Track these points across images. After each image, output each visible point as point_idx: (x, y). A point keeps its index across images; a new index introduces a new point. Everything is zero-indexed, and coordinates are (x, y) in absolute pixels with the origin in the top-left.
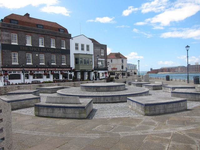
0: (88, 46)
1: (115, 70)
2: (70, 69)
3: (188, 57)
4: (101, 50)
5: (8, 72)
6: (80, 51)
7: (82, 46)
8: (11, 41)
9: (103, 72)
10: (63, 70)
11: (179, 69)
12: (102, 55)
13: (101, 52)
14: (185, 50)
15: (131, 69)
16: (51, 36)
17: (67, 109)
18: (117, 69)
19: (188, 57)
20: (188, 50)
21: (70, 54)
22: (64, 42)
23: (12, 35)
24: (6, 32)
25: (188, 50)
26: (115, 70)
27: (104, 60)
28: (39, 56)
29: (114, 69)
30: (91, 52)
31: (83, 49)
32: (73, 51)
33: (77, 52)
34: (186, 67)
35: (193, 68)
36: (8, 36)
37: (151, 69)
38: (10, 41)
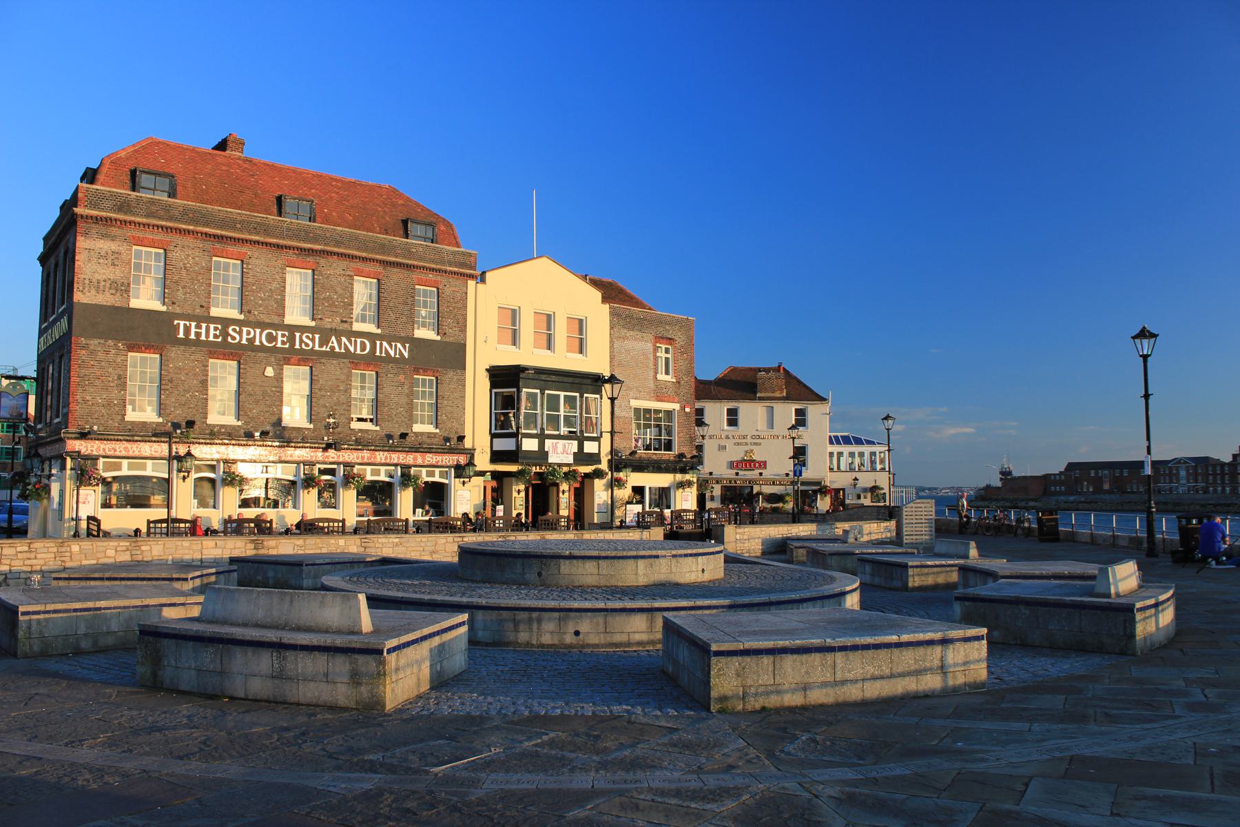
0: (580, 325)
1: (753, 474)
2: (463, 460)
3: (1147, 396)
4: (656, 349)
5: (102, 460)
6: (529, 355)
8: (127, 291)
9: (129, 408)
10: (419, 461)
11: (1183, 473)
12: (662, 377)
13: (656, 358)
14: (1130, 353)
15: (852, 470)
16: (360, 265)
17: (290, 655)
18: (763, 465)
19: (1147, 396)
20: (1145, 357)
22: (426, 294)
23: (138, 255)
24: (104, 236)
25: (1145, 357)
26: (753, 474)
27: (677, 406)
28: (279, 378)
29: (749, 464)
33: (508, 357)
34: (1223, 465)
35: (1223, 474)
36: (115, 259)
37: (1005, 474)
38: (123, 288)
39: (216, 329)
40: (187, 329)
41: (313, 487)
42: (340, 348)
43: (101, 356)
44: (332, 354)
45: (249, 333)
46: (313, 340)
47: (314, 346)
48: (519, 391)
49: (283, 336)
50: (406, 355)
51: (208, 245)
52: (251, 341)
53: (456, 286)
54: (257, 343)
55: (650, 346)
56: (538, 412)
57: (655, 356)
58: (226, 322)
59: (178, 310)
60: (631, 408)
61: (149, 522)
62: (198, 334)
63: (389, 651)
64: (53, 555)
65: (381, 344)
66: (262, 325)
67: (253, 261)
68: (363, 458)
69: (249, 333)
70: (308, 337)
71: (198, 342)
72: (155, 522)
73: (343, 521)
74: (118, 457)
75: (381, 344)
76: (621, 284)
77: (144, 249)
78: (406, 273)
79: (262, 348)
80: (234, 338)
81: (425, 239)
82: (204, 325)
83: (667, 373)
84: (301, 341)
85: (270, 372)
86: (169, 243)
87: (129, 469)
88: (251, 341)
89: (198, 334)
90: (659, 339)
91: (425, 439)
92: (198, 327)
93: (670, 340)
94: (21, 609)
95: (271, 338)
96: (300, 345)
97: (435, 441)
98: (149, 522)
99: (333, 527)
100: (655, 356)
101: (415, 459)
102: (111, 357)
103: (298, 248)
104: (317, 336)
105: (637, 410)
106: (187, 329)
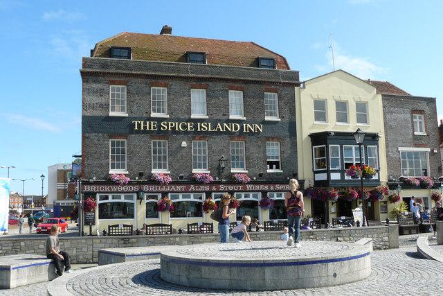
6: (332, 125)
7: (342, 106)
10: (272, 188)
16: (231, 84)
21: (296, 136)
24: (95, 82)
30: (375, 124)
31: (343, 118)
32: (308, 125)
33: (320, 128)
39: (154, 124)
40: (139, 125)
41: (308, 189)
42: (223, 129)
43: (96, 142)
44: (219, 133)
45: (172, 125)
46: (208, 126)
47: (208, 129)
48: (327, 147)
49: (191, 125)
50: (261, 130)
51: (148, 81)
52: (173, 129)
53: (288, 91)
54: (177, 129)
55: (408, 116)
56: (339, 157)
57: (413, 122)
58: (160, 120)
59: (134, 116)
60: (399, 152)
61: (109, 227)
62: (145, 127)
63: (14, 269)
64: (11, 248)
65: (246, 126)
66: (179, 120)
67: (173, 87)
68: (239, 188)
69: (172, 125)
70: (205, 125)
71: (145, 131)
72: (113, 226)
73: (171, 225)
74: (106, 193)
75: (246, 126)
76: (391, 83)
77: (116, 86)
78: (258, 86)
79: (179, 132)
80: (164, 128)
81: (269, 67)
82: (148, 123)
83: (421, 131)
84: (201, 127)
85: (184, 144)
86: (127, 82)
87: (113, 198)
88: (173, 129)
89: (145, 127)
90: (414, 111)
91: (275, 176)
92: (145, 123)
93: (421, 112)
94: (12, 267)
95: (185, 127)
96: (208, 125)
97: (280, 177)
98: (109, 227)
99: (159, 229)
100: (413, 122)
101: (269, 188)
102: (101, 142)
103: (196, 78)
104: (199, 130)
105: (403, 153)
106: (139, 125)
